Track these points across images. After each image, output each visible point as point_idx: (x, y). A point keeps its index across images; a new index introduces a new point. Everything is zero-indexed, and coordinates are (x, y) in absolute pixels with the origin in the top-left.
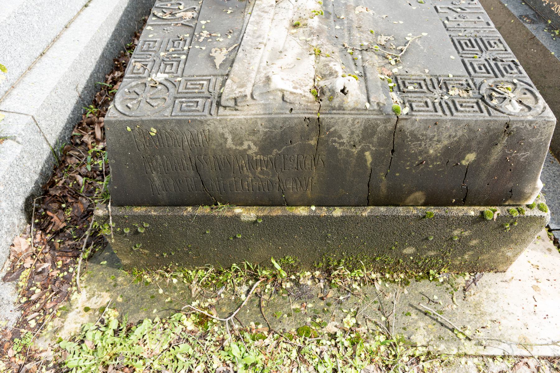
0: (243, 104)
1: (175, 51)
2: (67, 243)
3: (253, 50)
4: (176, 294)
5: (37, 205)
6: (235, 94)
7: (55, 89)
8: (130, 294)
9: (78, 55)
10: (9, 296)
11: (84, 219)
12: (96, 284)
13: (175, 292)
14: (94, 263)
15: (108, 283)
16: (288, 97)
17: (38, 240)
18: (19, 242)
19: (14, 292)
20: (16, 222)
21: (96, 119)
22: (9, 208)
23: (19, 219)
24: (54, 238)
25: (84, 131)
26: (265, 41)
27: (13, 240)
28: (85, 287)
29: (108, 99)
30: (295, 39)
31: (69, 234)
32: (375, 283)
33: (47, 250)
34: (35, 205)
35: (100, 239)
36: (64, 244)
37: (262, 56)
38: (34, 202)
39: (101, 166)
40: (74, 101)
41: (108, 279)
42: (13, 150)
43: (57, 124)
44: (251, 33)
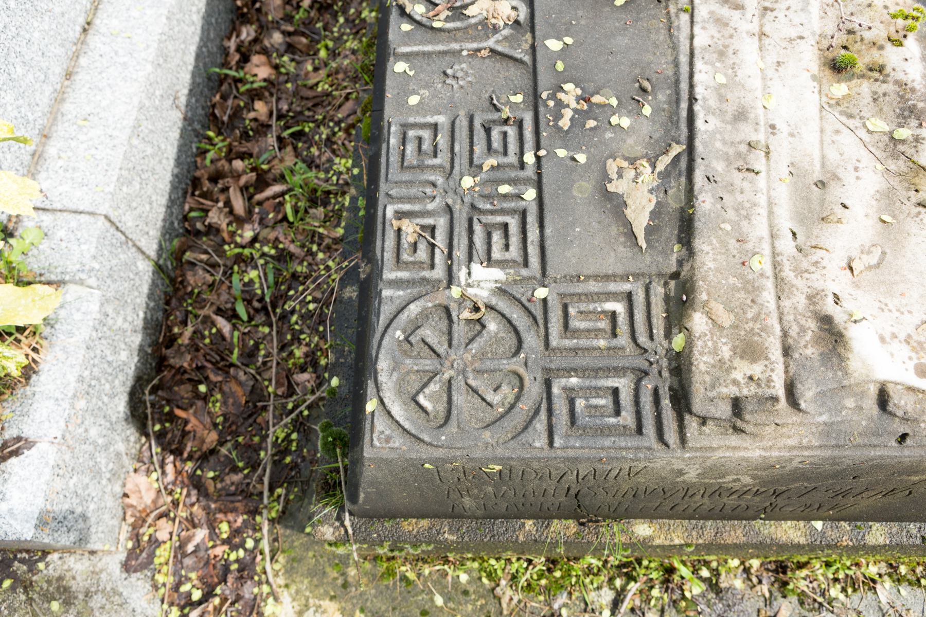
0: (761, 418)
1: (499, 166)
2: (228, 480)
3: (737, 177)
4: (470, 607)
5: (152, 397)
6: (735, 382)
7: (137, 126)
8: (379, 605)
9: (164, 20)
10: (144, 604)
11: (251, 421)
12: (306, 581)
13: (466, 602)
14: (292, 528)
15: (330, 580)
16: (900, 401)
17: (170, 477)
18: (137, 485)
19: (150, 596)
20: (121, 447)
21: (227, 167)
22: (104, 432)
23: (126, 439)
24: (200, 467)
25: (206, 198)
26: (760, 136)
27: (124, 485)
28: (287, 586)
29: (239, 105)
30: (851, 123)
31: (226, 456)
32: (878, 587)
33: (194, 499)
34: (148, 398)
35: (291, 469)
36: (222, 481)
37: (771, 204)
38: (147, 392)
39: (257, 285)
40: (175, 135)
41: (328, 569)
42: (83, 309)
43: (155, 204)
44: (713, 103)
